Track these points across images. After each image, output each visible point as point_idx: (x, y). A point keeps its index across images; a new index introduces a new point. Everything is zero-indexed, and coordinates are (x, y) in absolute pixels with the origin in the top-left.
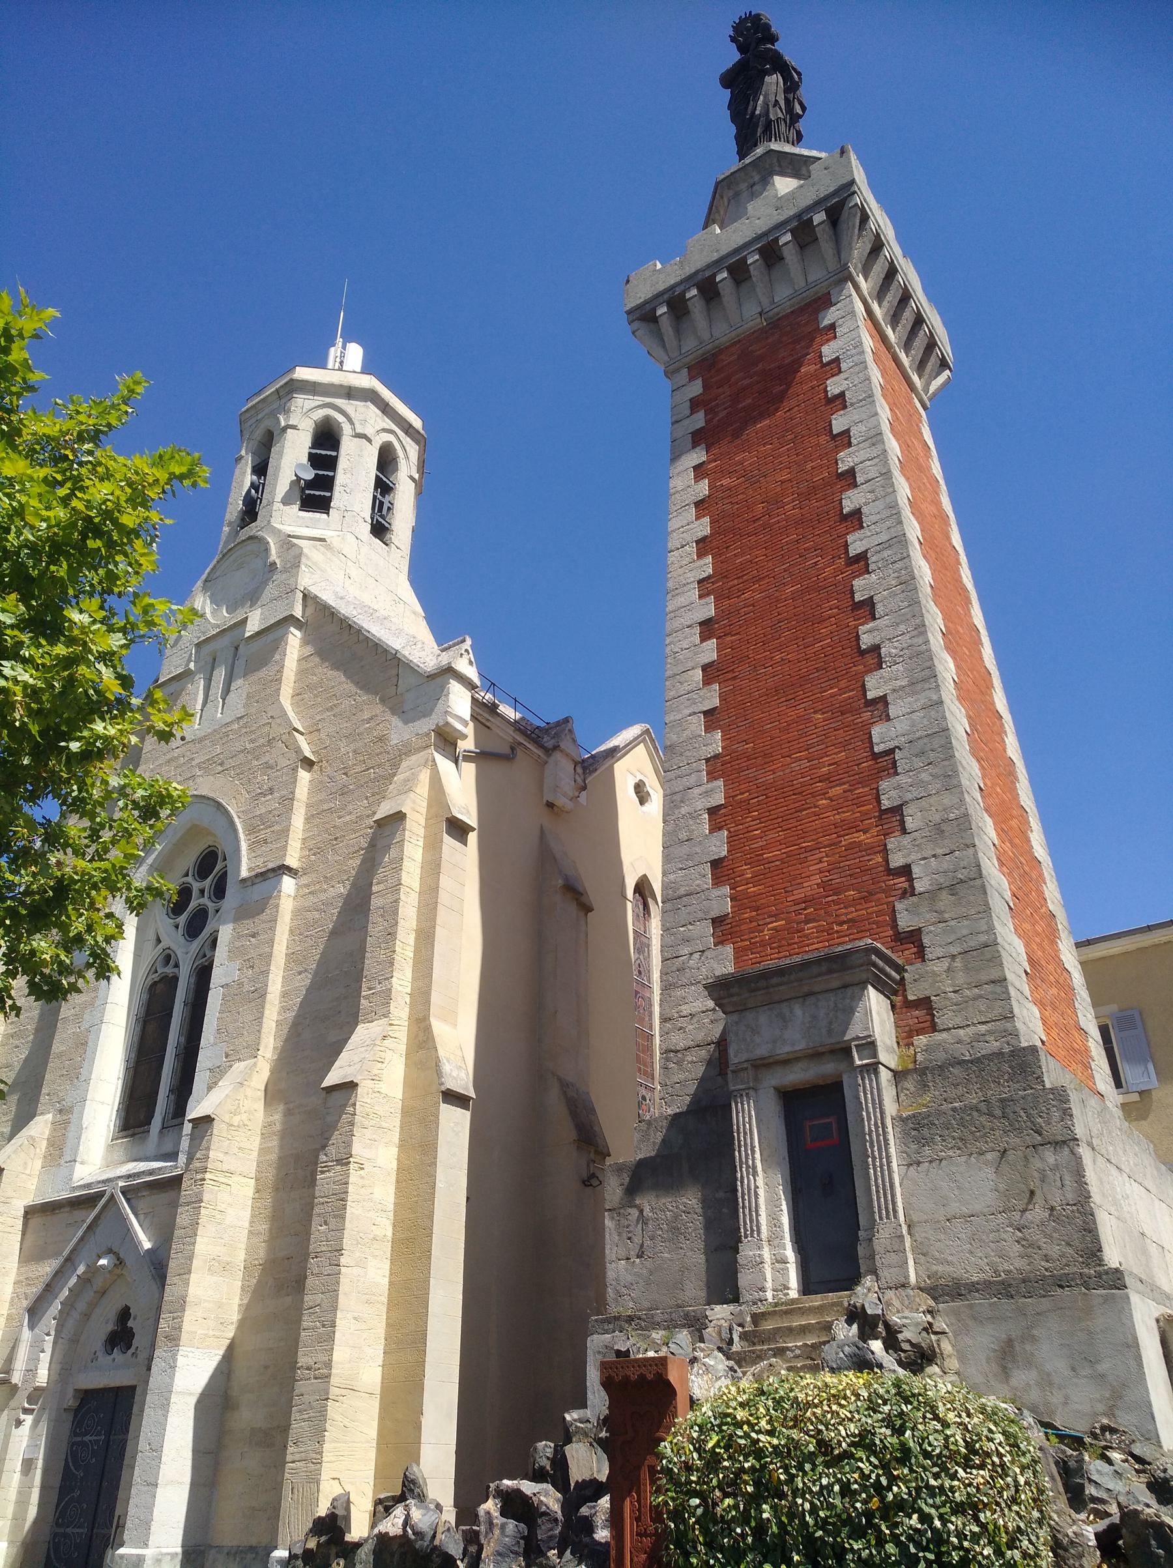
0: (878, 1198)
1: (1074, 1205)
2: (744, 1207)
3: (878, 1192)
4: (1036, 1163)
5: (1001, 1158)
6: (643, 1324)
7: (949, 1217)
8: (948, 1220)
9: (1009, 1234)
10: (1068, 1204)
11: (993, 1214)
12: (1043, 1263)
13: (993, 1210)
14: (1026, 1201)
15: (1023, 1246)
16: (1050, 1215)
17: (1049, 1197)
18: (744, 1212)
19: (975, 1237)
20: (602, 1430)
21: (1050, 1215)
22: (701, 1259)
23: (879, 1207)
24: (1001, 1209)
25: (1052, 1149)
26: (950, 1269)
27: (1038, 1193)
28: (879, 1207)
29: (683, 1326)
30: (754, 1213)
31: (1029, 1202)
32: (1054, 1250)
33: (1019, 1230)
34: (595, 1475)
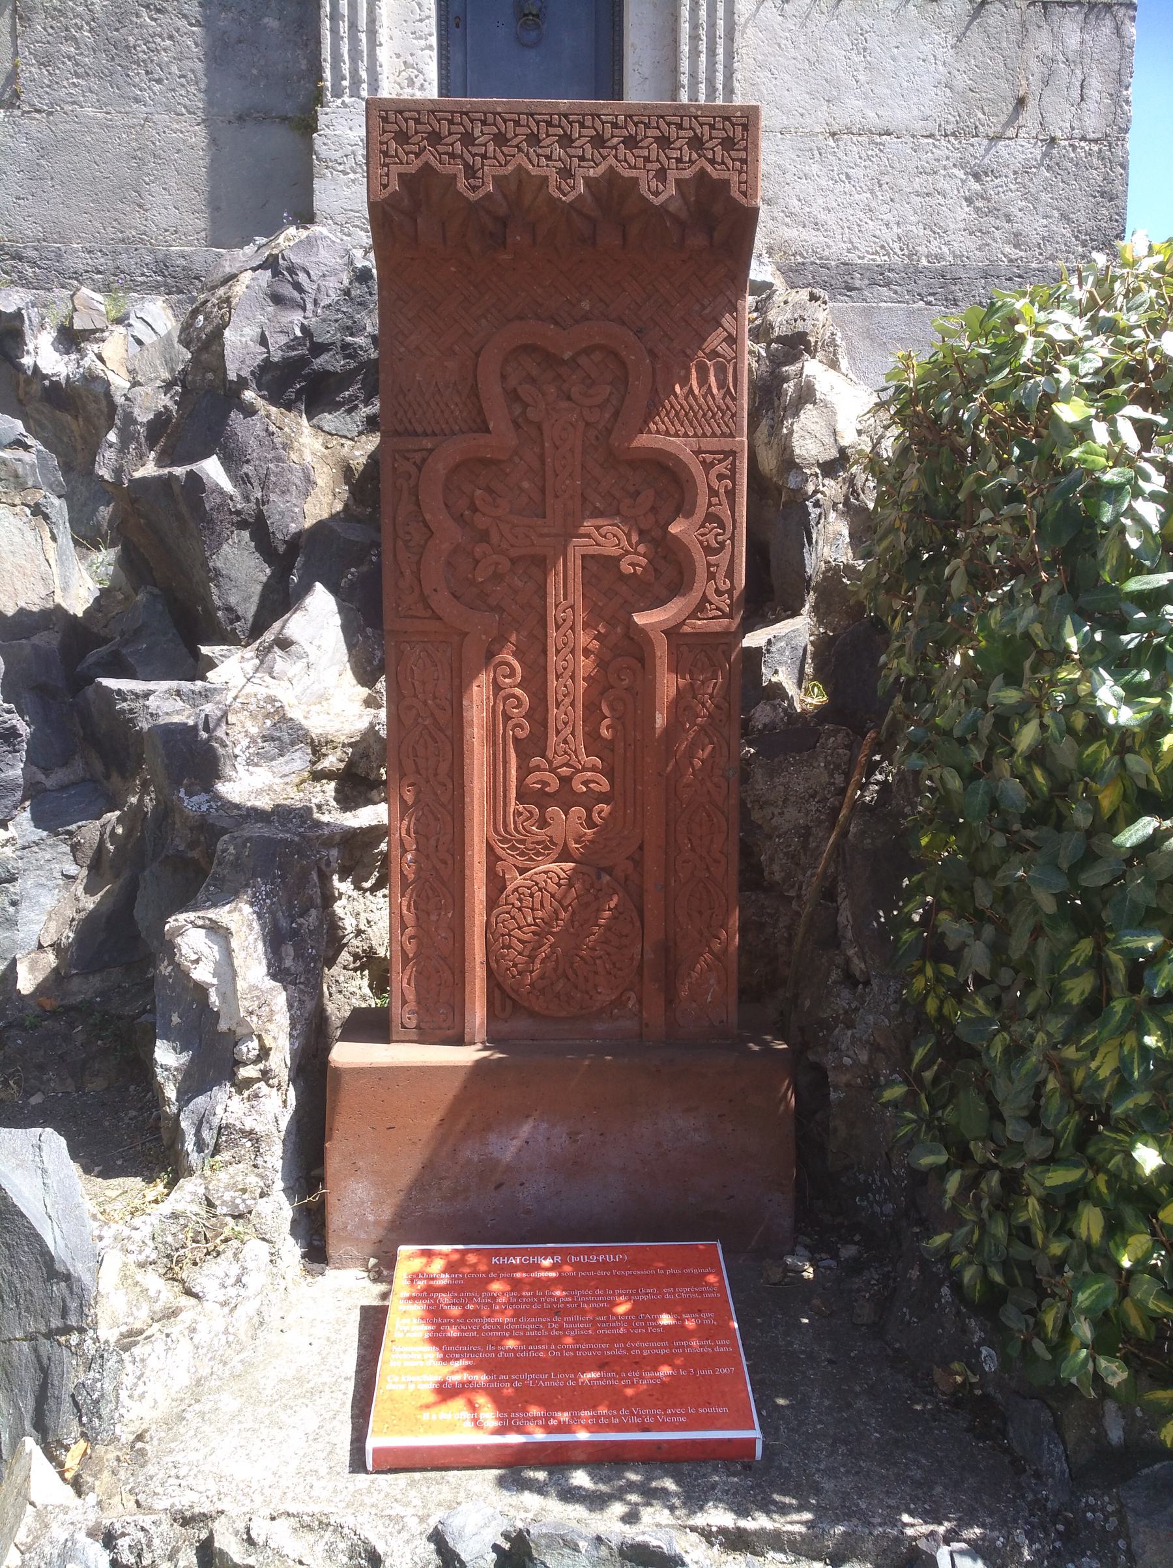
0: (695, 53)
1: (1096, 141)
2: (335, 16)
3: (694, 38)
4: (1042, 41)
5: (974, 17)
6: (29, 272)
7: (835, 128)
8: (833, 134)
9: (954, 183)
10: (1083, 139)
11: (931, 136)
12: (1008, 249)
13: (932, 127)
14: (1004, 118)
15: (977, 210)
16: (1045, 155)
17: (1050, 117)
18: (334, 31)
19: (886, 179)
20: (141, 457)
21: (1045, 155)
22: (197, 136)
23: (693, 75)
24: (950, 128)
25: (1081, 17)
26: (813, 237)
27: (1032, 104)
28: (693, 75)
29: (154, 288)
30: (363, 37)
31: (1010, 122)
32: (1034, 226)
33: (977, 177)
34: (58, 599)
